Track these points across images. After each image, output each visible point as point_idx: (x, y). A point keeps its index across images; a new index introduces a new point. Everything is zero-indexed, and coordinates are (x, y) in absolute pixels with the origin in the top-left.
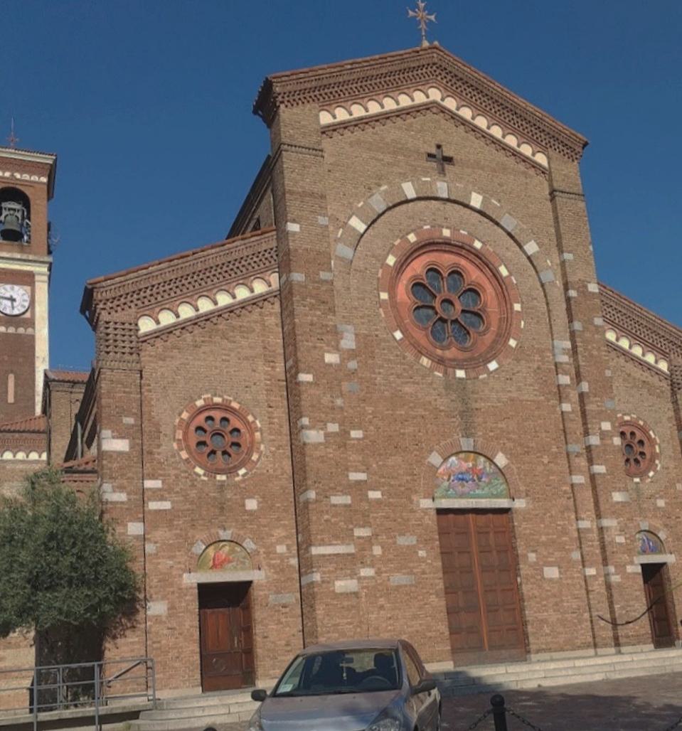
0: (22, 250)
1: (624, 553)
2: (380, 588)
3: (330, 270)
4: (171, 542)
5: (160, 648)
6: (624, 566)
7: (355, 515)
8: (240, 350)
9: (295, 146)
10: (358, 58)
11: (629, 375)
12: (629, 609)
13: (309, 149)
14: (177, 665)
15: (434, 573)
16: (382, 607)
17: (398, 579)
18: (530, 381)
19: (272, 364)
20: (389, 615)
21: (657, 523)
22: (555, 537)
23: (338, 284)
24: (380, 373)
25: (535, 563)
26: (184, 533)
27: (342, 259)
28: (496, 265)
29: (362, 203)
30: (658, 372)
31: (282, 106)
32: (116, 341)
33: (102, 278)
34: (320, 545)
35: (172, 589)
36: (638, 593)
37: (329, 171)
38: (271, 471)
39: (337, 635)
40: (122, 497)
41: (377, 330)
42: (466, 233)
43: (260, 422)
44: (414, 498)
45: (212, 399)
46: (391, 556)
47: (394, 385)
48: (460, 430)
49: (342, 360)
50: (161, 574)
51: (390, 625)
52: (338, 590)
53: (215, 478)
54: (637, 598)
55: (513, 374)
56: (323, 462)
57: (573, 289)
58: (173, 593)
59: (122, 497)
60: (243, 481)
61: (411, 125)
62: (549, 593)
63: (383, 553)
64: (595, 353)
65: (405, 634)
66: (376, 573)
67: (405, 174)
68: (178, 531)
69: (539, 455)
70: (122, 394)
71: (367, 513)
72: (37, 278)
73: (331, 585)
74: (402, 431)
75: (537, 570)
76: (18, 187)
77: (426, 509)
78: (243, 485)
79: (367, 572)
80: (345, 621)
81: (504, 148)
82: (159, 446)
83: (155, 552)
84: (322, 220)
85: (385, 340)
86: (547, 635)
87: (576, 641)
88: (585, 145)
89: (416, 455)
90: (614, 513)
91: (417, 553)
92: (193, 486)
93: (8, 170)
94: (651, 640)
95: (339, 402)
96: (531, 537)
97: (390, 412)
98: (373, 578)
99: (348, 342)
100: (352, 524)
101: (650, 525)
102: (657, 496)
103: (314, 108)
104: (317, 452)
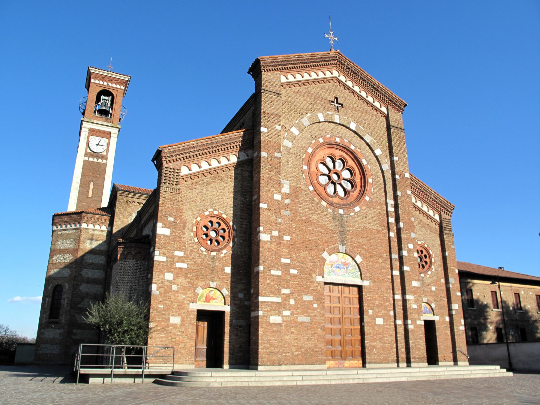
0: (107, 121)
2: (293, 322)
3: (280, 152)
4: (186, 285)
5: (175, 342)
6: (416, 320)
7: (282, 282)
8: (229, 188)
9: (268, 91)
10: (301, 53)
11: (421, 221)
12: (416, 343)
13: (275, 93)
14: (183, 351)
15: (321, 317)
16: (292, 333)
17: (302, 319)
18: (375, 219)
19: (245, 196)
20: (296, 338)
21: (431, 299)
22: (382, 302)
23: (283, 159)
24: (300, 207)
25: (371, 315)
26: (192, 281)
27: (286, 147)
28: (361, 159)
29: (298, 121)
31: (263, 72)
32: (169, 177)
33: (167, 146)
34: (264, 296)
35: (183, 311)
36: (422, 335)
37: (283, 104)
38: (239, 253)
39: (269, 345)
40: (163, 259)
41: (301, 184)
42: (347, 141)
43: (236, 226)
44: (314, 275)
45: (213, 212)
46: (299, 306)
47: (307, 214)
48: (339, 241)
49: (283, 198)
50: (179, 302)
51: (296, 343)
52: (271, 322)
53: (210, 254)
54: (420, 338)
55: (367, 214)
56: (268, 251)
57: (398, 174)
58: (184, 313)
59: (163, 259)
60: (225, 257)
61: (324, 87)
62: (378, 332)
63: (295, 303)
65: (303, 348)
66: (291, 314)
67: (319, 109)
68: (190, 280)
69: (378, 258)
70: (169, 205)
71: (289, 281)
73: (268, 318)
74: (310, 239)
75: (372, 319)
77: (319, 282)
78: (224, 259)
79: (287, 313)
80: (274, 338)
81: (368, 103)
82: (184, 234)
83: (177, 290)
84: (279, 128)
85: (304, 190)
86: (375, 354)
87: (389, 359)
88: (406, 105)
89: (316, 252)
91: (313, 305)
92: (199, 256)
94: (426, 361)
95: (280, 220)
96: (371, 301)
97: (305, 228)
98: (289, 316)
99: (286, 189)
100: (281, 286)
101: (428, 300)
102: (432, 284)
103: (279, 74)
104: (266, 246)
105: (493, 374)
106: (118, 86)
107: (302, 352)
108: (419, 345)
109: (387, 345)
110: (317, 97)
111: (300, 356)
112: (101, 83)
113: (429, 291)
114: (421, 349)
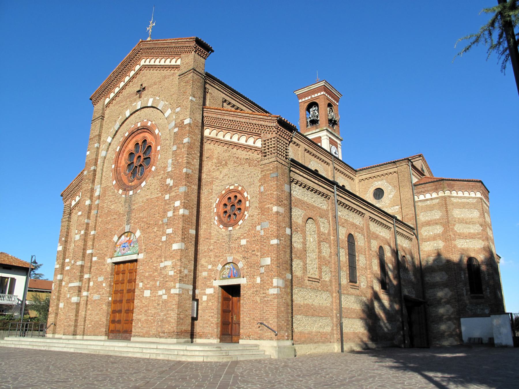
0: (317, 128)
1: (172, 281)
12: (167, 316)
22: (152, 273)
30: (256, 149)
64: (180, 160)
69: (153, 227)
72: (322, 138)
76: (314, 101)
86: (139, 327)
90: (171, 257)
93: (309, 96)
105: (155, 355)
106: (319, 94)
107: (92, 325)
108: (170, 317)
109: (150, 317)
110: (129, 96)
111: (91, 328)
112: (307, 99)
113: (237, 246)
114: (172, 322)
